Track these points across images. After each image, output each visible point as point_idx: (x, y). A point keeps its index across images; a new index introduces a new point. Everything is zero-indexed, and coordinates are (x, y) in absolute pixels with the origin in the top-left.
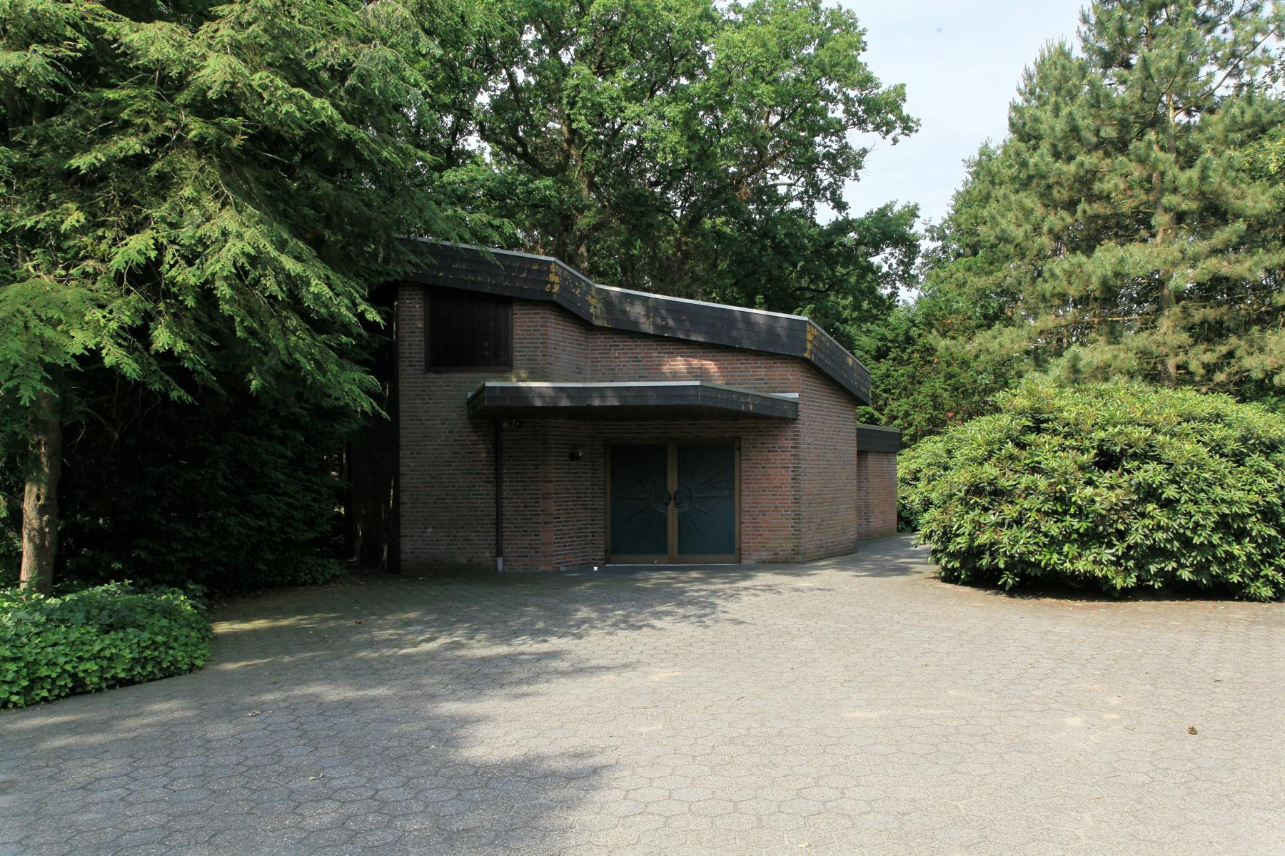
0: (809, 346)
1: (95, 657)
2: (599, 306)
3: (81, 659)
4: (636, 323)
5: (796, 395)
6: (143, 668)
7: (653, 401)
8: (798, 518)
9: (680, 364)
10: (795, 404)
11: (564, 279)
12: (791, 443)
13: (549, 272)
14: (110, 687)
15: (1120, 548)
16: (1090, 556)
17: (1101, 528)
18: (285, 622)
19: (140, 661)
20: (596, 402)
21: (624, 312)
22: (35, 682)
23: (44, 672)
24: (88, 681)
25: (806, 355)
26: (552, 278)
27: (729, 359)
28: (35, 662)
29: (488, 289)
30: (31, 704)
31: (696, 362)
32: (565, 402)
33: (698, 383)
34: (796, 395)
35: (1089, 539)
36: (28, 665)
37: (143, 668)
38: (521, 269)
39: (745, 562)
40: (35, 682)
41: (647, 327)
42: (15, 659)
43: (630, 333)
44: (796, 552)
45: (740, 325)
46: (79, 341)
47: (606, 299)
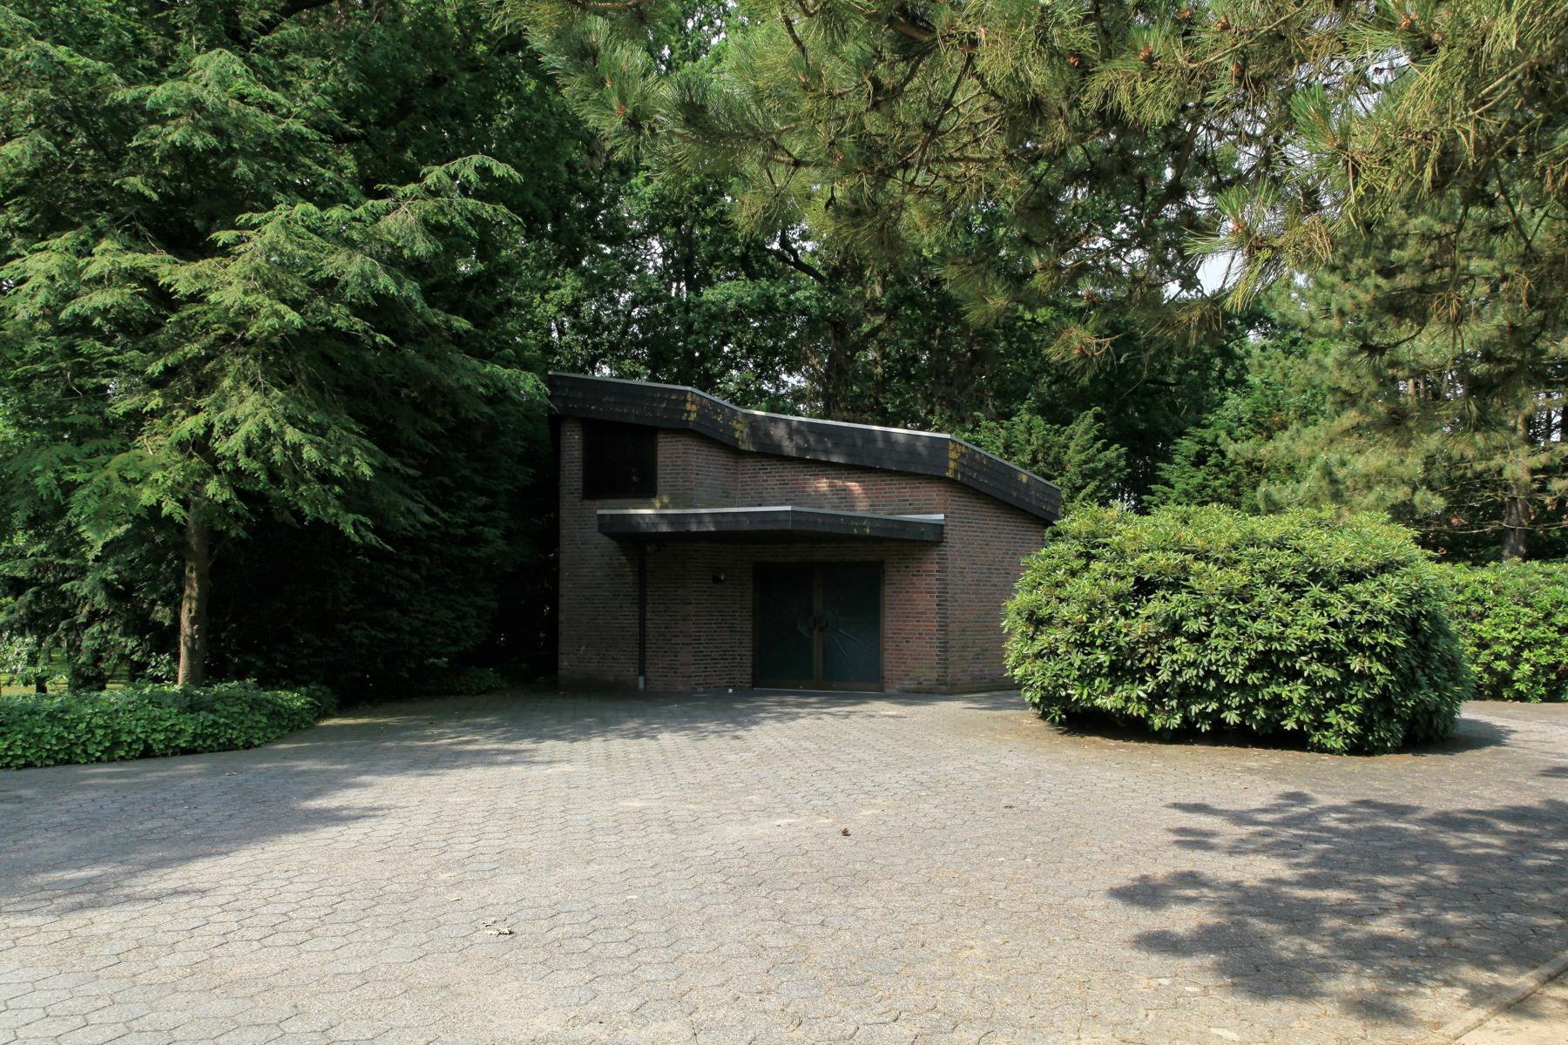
0: (952, 465)
1: (166, 730)
2: (746, 430)
3: (154, 730)
4: (779, 446)
5: (941, 517)
6: (204, 741)
7: (746, 526)
8: (944, 647)
9: (823, 485)
10: (939, 528)
11: (703, 407)
12: (936, 567)
13: (686, 401)
14: (174, 754)
15: (1151, 685)
16: (1121, 692)
17: (1129, 663)
18: (360, 721)
19: (195, 736)
20: (694, 528)
21: (768, 435)
22: (116, 744)
23: (124, 737)
24: (155, 747)
25: (949, 474)
26: (689, 407)
27: (866, 477)
28: (119, 731)
29: (633, 420)
30: (111, 760)
31: (839, 483)
32: (664, 528)
33: (789, 508)
34: (941, 517)
35: (1119, 672)
36: (114, 732)
37: (204, 741)
38: (662, 400)
39: (888, 691)
40: (116, 744)
41: (789, 448)
42: (106, 727)
43: (769, 454)
44: (941, 682)
45: (880, 444)
46: (147, 496)
47: (753, 422)
